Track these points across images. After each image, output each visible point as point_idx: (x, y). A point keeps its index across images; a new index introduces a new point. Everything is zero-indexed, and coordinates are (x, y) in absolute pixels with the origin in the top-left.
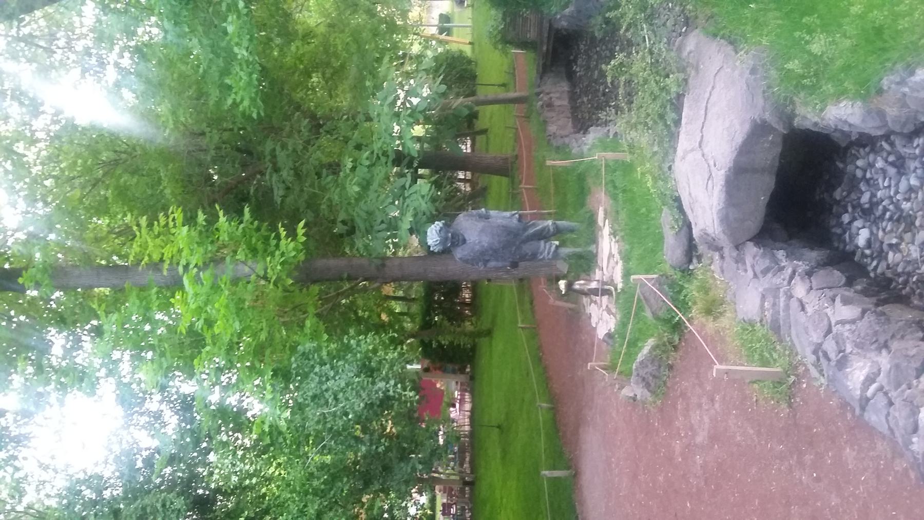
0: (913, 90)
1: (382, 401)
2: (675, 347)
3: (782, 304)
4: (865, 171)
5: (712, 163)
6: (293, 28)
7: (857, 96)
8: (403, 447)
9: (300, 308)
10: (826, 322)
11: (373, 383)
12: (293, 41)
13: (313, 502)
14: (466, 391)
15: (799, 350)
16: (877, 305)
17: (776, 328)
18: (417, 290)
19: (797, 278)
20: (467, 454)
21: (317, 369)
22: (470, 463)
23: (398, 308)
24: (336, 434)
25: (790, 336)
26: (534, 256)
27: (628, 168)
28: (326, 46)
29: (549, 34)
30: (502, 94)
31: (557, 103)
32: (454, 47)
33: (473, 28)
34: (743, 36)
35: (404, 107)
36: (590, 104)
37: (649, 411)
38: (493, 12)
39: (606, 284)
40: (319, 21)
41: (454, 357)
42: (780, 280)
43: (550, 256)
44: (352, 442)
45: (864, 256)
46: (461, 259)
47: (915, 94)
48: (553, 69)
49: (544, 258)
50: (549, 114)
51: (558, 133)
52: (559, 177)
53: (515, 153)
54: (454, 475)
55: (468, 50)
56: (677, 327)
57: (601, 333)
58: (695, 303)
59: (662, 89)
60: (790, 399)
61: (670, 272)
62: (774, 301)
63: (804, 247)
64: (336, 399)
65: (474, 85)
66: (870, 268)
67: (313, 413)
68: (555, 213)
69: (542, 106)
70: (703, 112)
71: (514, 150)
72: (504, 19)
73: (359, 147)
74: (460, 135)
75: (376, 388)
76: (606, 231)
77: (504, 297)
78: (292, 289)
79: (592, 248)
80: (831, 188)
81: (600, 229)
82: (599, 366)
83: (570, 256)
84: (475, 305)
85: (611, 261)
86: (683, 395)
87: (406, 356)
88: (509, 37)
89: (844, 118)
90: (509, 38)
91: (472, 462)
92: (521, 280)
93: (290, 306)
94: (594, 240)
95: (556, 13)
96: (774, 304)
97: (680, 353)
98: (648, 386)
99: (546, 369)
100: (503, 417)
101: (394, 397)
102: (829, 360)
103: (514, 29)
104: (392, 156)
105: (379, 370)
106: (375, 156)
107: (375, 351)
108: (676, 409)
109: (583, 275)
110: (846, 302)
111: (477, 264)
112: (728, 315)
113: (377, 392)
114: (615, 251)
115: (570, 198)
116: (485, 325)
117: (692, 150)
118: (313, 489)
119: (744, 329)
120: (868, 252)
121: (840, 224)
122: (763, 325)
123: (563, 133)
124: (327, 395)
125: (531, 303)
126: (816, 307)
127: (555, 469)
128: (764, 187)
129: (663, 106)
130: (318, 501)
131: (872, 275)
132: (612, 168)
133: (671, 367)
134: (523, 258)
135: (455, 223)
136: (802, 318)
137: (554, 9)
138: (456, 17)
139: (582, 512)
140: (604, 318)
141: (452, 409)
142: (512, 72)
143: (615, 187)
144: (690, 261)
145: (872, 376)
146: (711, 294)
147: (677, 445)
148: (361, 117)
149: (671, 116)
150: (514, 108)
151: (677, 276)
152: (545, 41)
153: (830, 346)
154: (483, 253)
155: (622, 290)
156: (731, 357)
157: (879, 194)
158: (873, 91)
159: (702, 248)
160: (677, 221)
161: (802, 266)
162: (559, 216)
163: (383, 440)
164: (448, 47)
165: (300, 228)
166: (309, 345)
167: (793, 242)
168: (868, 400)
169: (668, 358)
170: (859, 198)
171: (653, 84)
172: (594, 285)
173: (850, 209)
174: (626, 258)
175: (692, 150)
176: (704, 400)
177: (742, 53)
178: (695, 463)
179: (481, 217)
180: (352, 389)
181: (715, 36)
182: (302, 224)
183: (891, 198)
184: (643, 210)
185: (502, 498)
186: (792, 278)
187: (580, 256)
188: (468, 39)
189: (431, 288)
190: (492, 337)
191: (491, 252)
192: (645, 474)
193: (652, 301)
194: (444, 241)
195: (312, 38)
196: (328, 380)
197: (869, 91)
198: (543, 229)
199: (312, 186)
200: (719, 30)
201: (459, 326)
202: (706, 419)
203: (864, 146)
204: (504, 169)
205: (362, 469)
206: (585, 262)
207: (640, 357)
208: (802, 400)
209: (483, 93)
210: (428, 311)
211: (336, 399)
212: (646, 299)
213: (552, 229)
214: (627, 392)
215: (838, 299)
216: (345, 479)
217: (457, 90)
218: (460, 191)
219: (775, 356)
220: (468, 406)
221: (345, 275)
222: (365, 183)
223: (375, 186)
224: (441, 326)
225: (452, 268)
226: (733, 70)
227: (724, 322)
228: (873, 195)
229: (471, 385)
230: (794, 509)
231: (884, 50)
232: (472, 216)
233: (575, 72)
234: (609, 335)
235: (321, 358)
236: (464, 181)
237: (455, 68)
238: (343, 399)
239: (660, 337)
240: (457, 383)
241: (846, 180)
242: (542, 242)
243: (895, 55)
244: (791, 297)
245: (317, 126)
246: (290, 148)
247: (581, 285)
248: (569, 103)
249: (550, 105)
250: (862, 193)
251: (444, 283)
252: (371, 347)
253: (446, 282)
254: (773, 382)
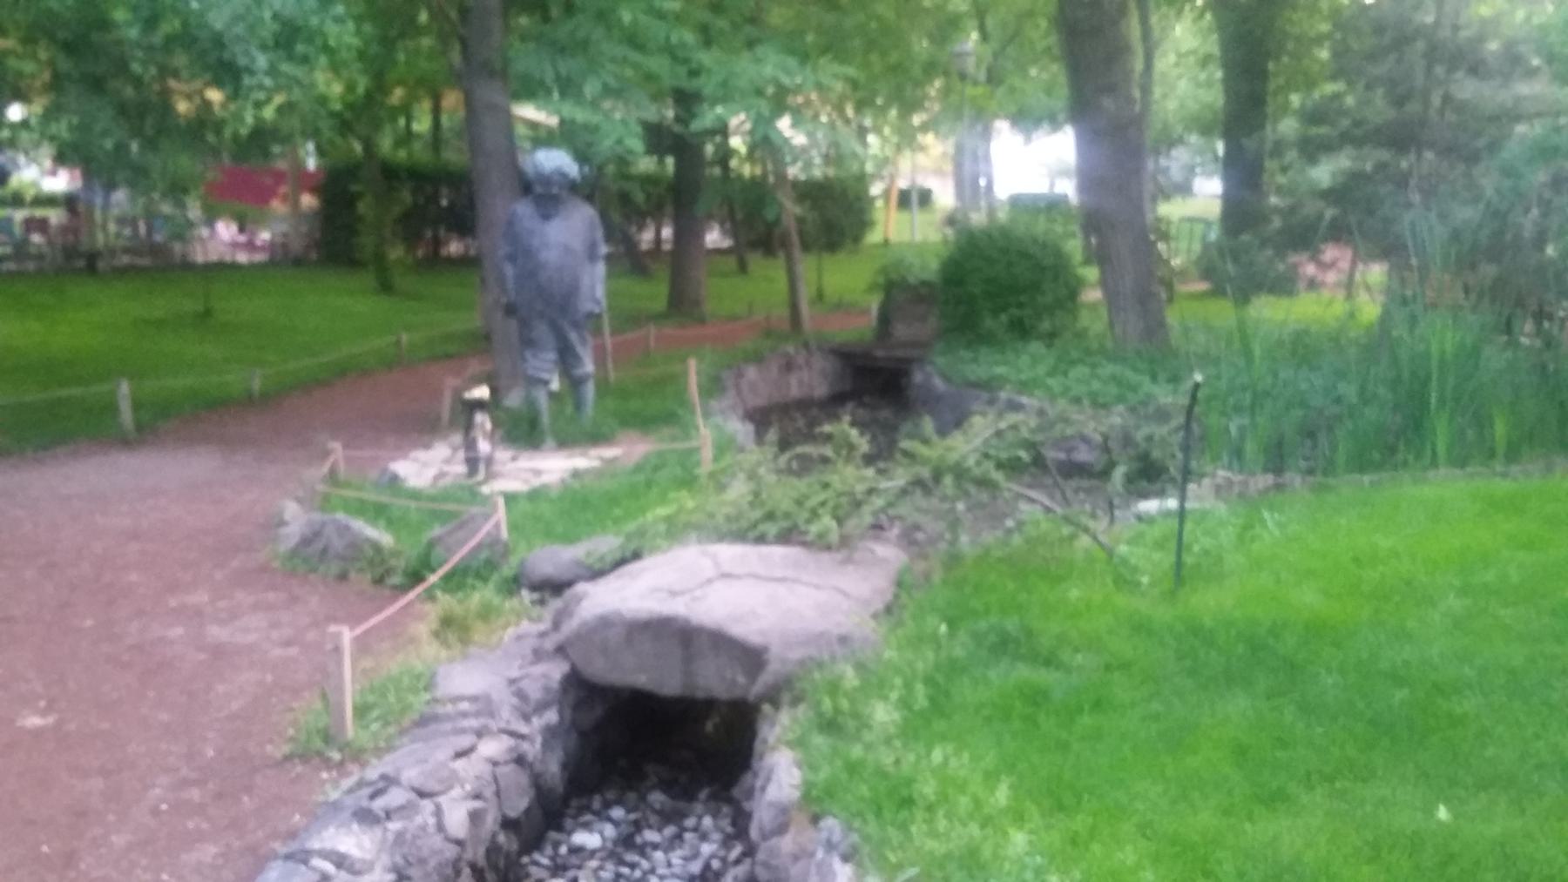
0: (819, 866)
4: (695, 830)
7: (807, 787)
10: (437, 788)
11: (264, 47)
16: (474, 868)
17: (424, 721)
18: (454, 156)
23: (422, 125)
26: (528, 343)
27: (688, 481)
30: (806, 293)
31: (793, 380)
36: (786, 422)
38: (934, 265)
41: (335, 241)
42: (507, 716)
43: (530, 372)
45: (556, 845)
47: (813, 870)
52: (670, 383)
55: (874, 237)
56: (416, 578)
58: (460, 602)
61: (514, 561)
62: (474, 708)
63: (566, 754)
66: (537, 856)
70: (779, 573)
72: (924, 283)
74: (733, 227)
77: (455, 311)
80: (667, 786)
81: (584, 455)
84: (435, 261)
86: (294, 600)
88: (901, 294)
89: (774, 777)
94: (565, 442)
98: (306, 541)
102: (373, 797)
107: (326, 49)
110: (475, 817)
112: (444, 653)
114: (546, 479)
115: (635, 404)
119: (418, 677)
120: (563, 850)
121: (607, 805)
122: (428, 703)
128: (660, 676)
129: (787, 515)
131: (525, 860)
132: (688, 458)
134: (525, 324)
137: (940, 361)
143: (656, 468)
145: (347, 863)
147: (200, 597)
149: (772, 529)
150: (783, 312)
151: (507, 570)
153: (396, 797)
156: (367, 663)
157: (659, 855)
158: (816, 809)
159: (556, 604)
161: (532, 750)
162: (603, 388)
164: (879, 204)
167: (574, 736)
168: (305, 862)
170: (650, 827)
171: (822, 497)
172: (484, 446)
173: (633, 816)
174: (535, 495)
176: (287, 632)
181: (899, 584)
183: (653, 871)
188: (894, 237)
194: (546, 180)
197: (813, 805)
198: (577, 358)
202: (251, 638)
203: (734, 824)
204: (682, 303)
206: (524, 432)
208: (298, 776)
209: (807, 266)
214: (291, 509)
215: (477, 804)
220: (242, 258)
223: (635, 56)
225: (503, 209)
228: (655, 847)
229: (283, 260)
230: (97, 783)
231: (879, 813)
234: (395, 479)
239: (396, 554)
241: (681, 805)
243: (872, 828)
249: (789, 366)
250: (660, 830)
251: (471, 204)
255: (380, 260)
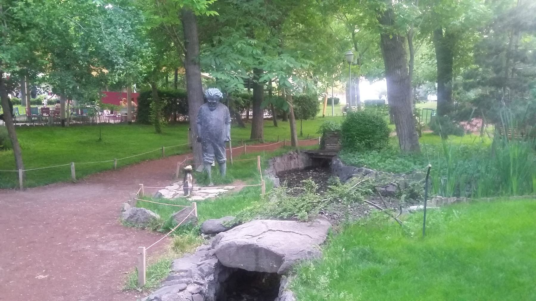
1: (111, 61)
2: (156, 229)
3: (183, 280)
5: (260, 236)
6: (329, 14)
8: (83, 78)
9: (166, 11)
11: (122, 56)
12: (322, 12)
13: (44, 20)
14: (122, 120)
15: (157, 291)
17: (169, 279)
18: (182, 89)
19: (198, 286)
20: (82, 122)
21: (128, 22)
22: (77, 124)
23: (171, 79)
24: (88, 35)
25: (165, 286)
26: (205, 151)
28: (319, 33)
29: (329, 156)
30: (297, 133)
32: (321, 107)
33: (332, 117)
34: (329, 248)
35: (288, 78)
36: (290, 177)
37: (116, 219)
39: (191, 192)
40: (333, 29)
41: (143, 116)
42: (197, 277)
44: (84, 45)
46: (201, 108)
48: (311, 159)
49: (204, 156)
50: (286, 158)
51: (276, 163)
52: (251, 164)
53: (264, 142)
54: (68, 114)
55: (320, 114)
57: (163, 192)
59: (299, 209)
60: (128, 290)
61: (199, 224)
64: (110, 34)
65: (301, 118)
67: (101, 20)
68: (230, 162)
69: (290, 154)
71: (266, 141)
72: (337, 131)
73: (264, 49)
75: (119, 58)
76: (222, 191)
77: (181, 139)
78: (178, 8)
79: (212, 184)
82: (141, 190)
83: (206, 171)
84: (175, 123)
85: (205, 194)
86: (127, 236)
87: (140, 77)
88: (328, 135)
90: (326, 134)
91: (76, 124)
92: (191, 148)
93: (167, 7)
94: (216, 184)
95: (339, 158)
96: (183, 277)
97: (152, 233)
98: (131, 217)
99: (137, 163)
100: (107, 141)
101: (114, 69)
103: (331, 137)
104: (259, 67)
105: (130, 60)
106: (259, 57)
107: (142, 57)
108: (119, 232)
109: (195, 180)
111: (199, 118)
113: (116, 58)
114: (210, 196)
116: (163, 129)
117: (267, 227)
118: (52, 21)
119: (167, 263)
123: (276, 166)
124: (113, 28)
125: (178, 154)
126: (182, 297)
127: (76, 171)
129: (291, 210)
130: (45, 24)
133: (143, 229)
134: (204, 144)
135: (222, 105)
136: (176, 290)
138: (337, 108)
139: (51, 187)
140: (170, 193)
141: (109, 112)
142: (308, 138)
143: (246, 193)
144: (206, 234)
146: (188, 245)
147: (96, 235)
148: (280, 50)
149: (285, 215)
150: (290, 140)
151: (197, 227)
152: (326, 154)
154: (206, 121)
155: (188, 201)
156: (151, 258)
159: (213, 239)
160: (228, 224)
162: (229, 165)
163: (86, 63)
165: (214, 13)
166: (143, 17)
169: (149, 226)
172: (190, 185)
174: (206, 201)
175: (267, 227)
177: (319, 248)
178: (86, 245)
179: (227, 119)
180: (117, 43)
182: (217, 14)
184: (234, 207)
185: (55, 143)
186: (198, 283)
187: (206, 177)
188: (326, 115)
189: (184, 97)
190: (155, 133)
191: (206, 126)
192: (77, 220)
193: (182, 215)
194: (212, 98)
195: (324, 24)
196: (123, 28)
199: (240, 21)
200: (331, 236)
201: (162, 114)
204: (255, 136)
205: (67, 52)
206: (203, 180)
207: (149, 211)
208: (128, 296)
209: (297, 124)
210: (170, 95)
211: (110, 34)
212: (182, 212)
213: (221, 160)
214: (127, 206)
216: (59, 41)
217: (298, 109)
218: (242, 112)
219: (153, 280)
220: (112, 121)
221: (187, 41)
222: (242, 52)
224: (160, 103)
226: (310, 244)
227: (172, 254)
229: (125, 122)
232: (227, 114)
233: (309, 171)
235: (136, 24)
236: (248, 115)
237: (310, 107)
238: (110, 38)
239: (160, 221)
240: (126, 114)
242: (213, 155)
244: (188, 284)
245: (275, 25)
246: (261, 8)
247: (190, 177)
248: (293, 169)
249: (291, 158)
252: (144, 54)
253: (188, 106)
254: (137, 280)
255: (157, 122)
